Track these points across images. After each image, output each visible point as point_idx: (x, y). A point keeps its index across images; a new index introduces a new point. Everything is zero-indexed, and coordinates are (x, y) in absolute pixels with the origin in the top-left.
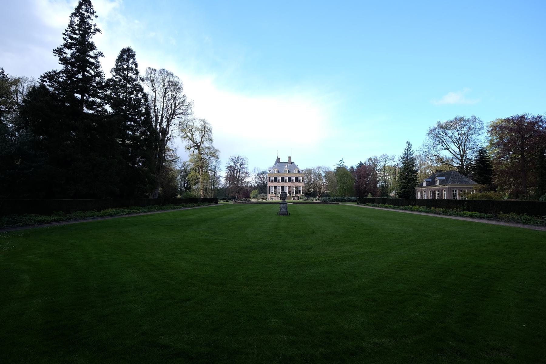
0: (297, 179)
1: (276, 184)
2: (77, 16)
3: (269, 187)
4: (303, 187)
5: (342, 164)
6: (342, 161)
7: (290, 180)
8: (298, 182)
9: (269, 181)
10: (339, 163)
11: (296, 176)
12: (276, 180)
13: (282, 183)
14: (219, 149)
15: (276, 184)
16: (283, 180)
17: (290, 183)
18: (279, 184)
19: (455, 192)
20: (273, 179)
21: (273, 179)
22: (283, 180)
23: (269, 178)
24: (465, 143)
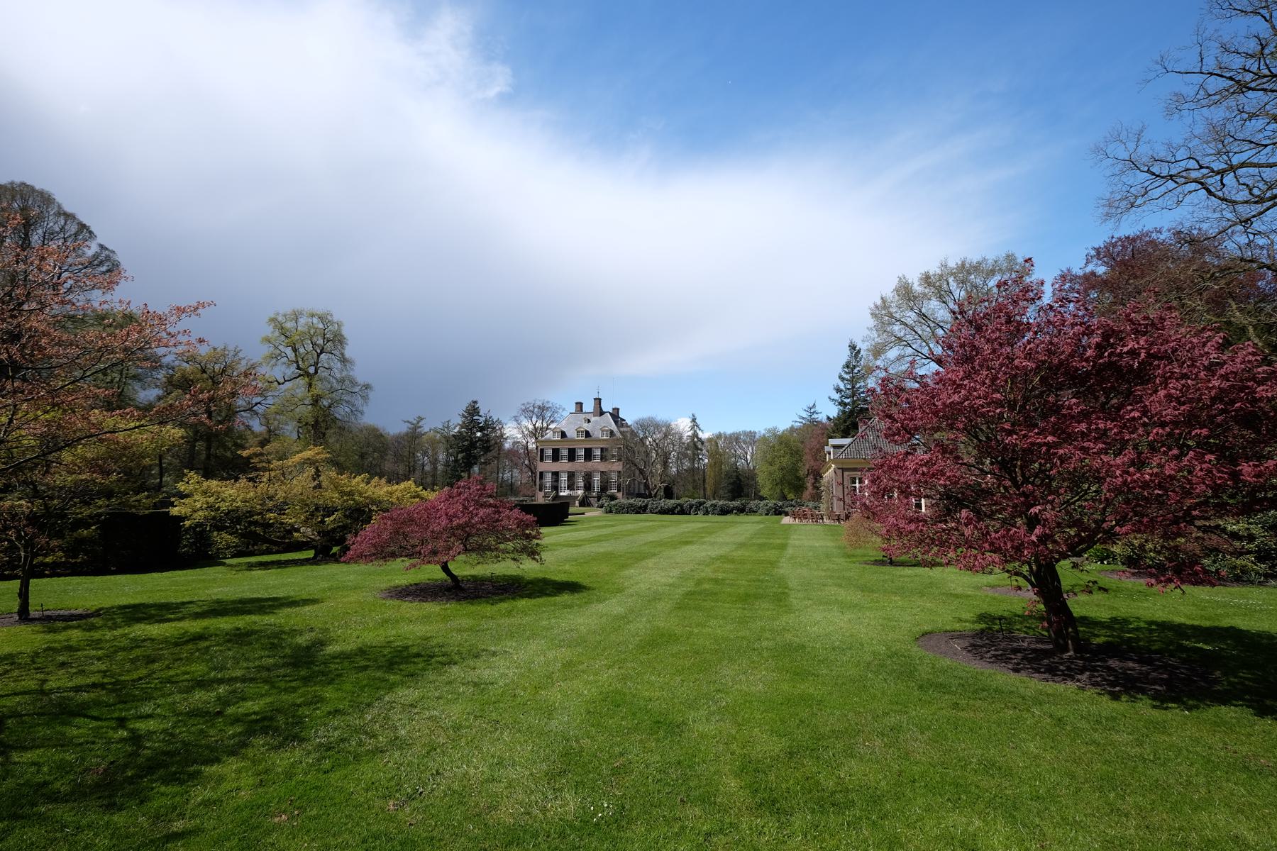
0: (588, 455)
1: (556, 467)
2: (1083, 422)
3: (541, 474)
4: (619, 472)
5: (815, 416)
6: (812, 410)
7: (588, 455)
8: (590, 460)
9: (542, 460)
10: (805, 415)
11: (571, 447)
12: (556, 456)
13: (571, 463)
14: (469, 400)
15: (556, 467)
16: (572, 456)
17: (590, 464)
18: (580, 465)
19: (857, 485)
20: (565, 453)
21: (549, 453)
22: (572, 456)
23: (542, 451)
24: (929, 347)
